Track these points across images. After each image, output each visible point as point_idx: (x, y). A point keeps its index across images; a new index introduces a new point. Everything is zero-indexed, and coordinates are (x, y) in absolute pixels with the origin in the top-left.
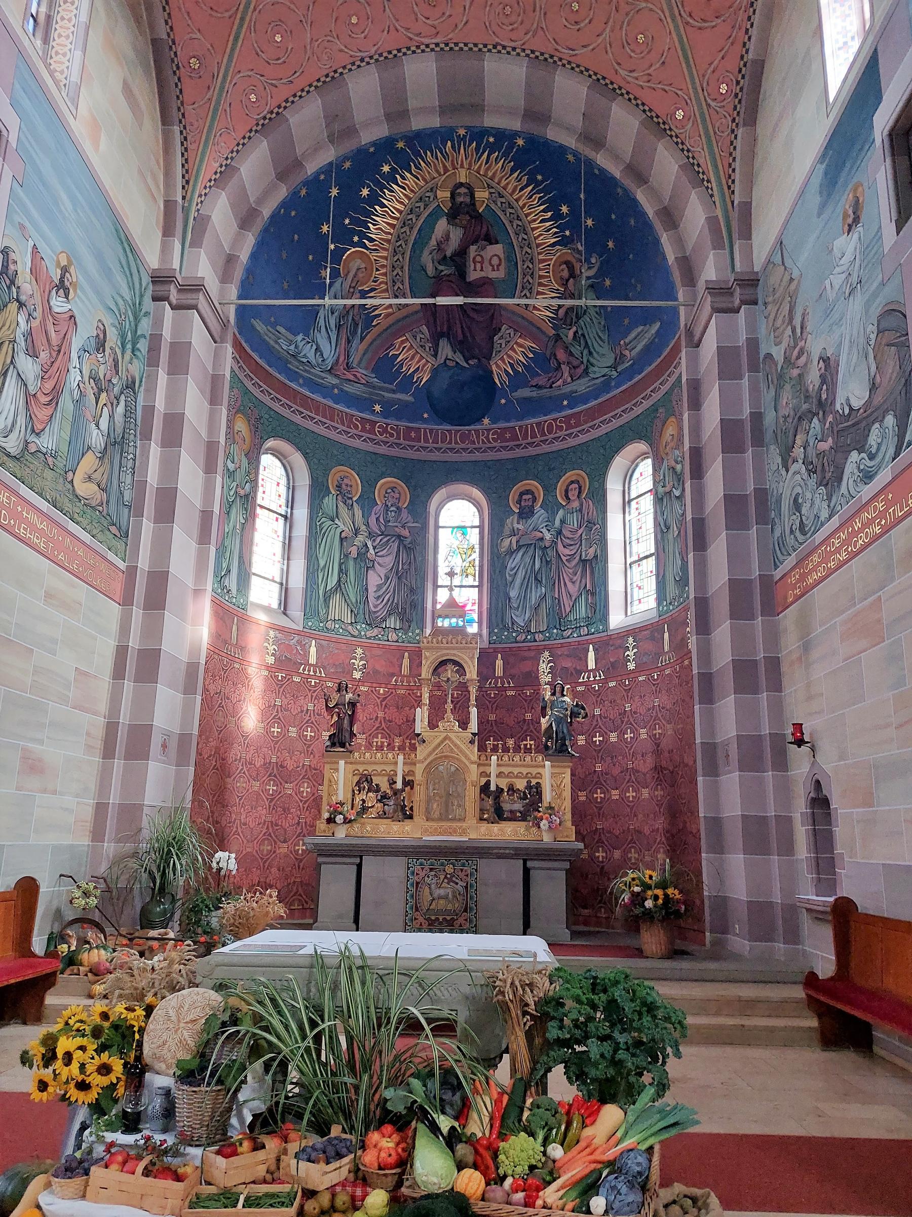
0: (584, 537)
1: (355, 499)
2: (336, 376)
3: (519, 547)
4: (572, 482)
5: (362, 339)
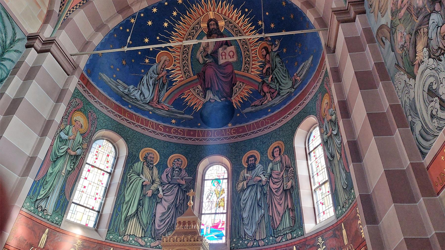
0: (284, 176)
1: (154, 165)
2: (152, 106)
3: (248, 187)
4: (276, 148)
5: (167, 91)
